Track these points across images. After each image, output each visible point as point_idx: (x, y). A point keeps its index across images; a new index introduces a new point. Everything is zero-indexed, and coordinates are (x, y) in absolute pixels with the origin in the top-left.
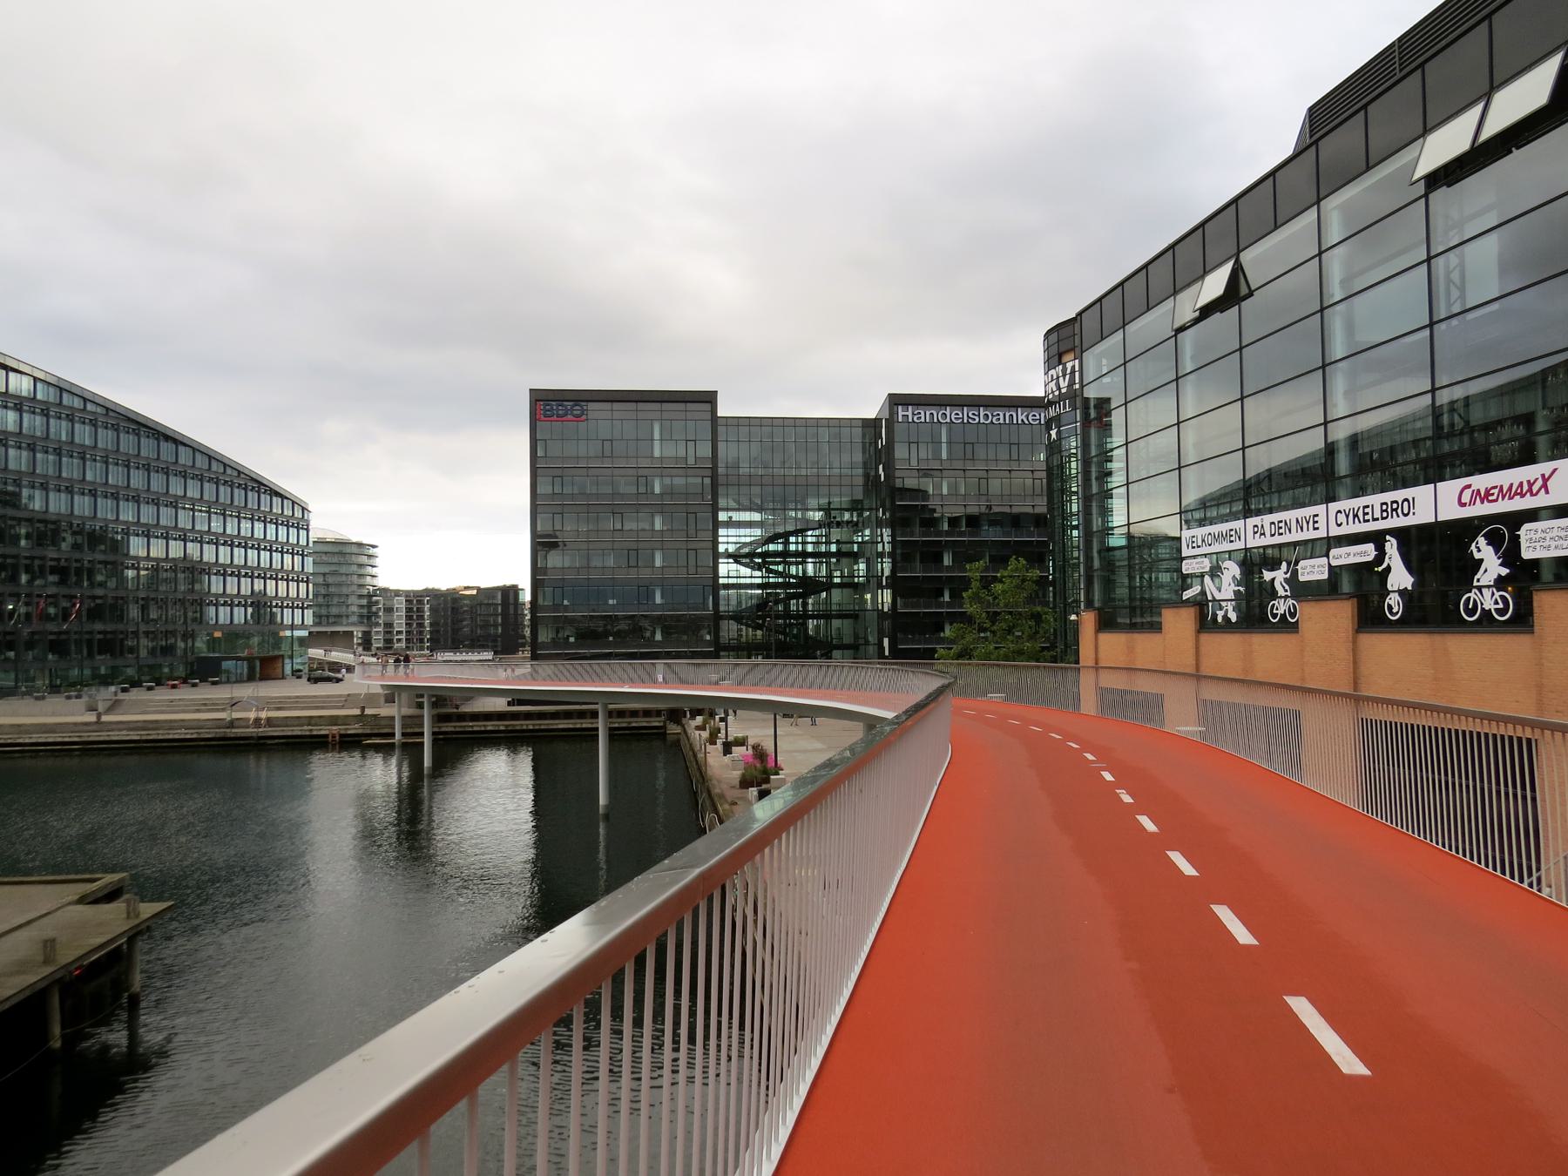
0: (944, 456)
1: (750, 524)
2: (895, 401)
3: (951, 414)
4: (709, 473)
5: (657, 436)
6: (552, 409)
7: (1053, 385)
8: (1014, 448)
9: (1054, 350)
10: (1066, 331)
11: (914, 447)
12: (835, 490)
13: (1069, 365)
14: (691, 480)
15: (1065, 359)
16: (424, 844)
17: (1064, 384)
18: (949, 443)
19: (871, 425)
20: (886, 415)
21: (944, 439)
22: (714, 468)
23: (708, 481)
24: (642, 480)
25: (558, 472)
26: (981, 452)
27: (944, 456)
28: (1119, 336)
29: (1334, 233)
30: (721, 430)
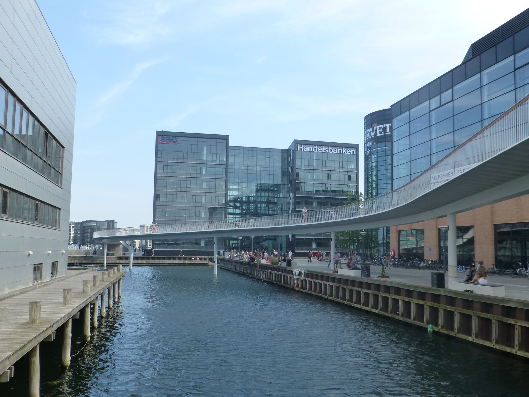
0: (315, 164)
2: (297, 142)
3: (318, 149)
4: (225, 167)
5: (205, 151)
6: (163, 138)
7: (368, 135)
8: (341, 163)
9: (370, 122)
10: (160, 181)
11: (303, 160)
12: (267, 176)
13: (375, 128)
14: (217, 169)
15: (373, 126)
16: (121, 310)
17: (373, 134)
18: (317, 159)
21: (315, 158)
23: (224, 170)
24: (199, 168)
25: (166, 164)
26: (328, 164)
27: (315, 164)
28: (408, 113)
29: (485, 82)
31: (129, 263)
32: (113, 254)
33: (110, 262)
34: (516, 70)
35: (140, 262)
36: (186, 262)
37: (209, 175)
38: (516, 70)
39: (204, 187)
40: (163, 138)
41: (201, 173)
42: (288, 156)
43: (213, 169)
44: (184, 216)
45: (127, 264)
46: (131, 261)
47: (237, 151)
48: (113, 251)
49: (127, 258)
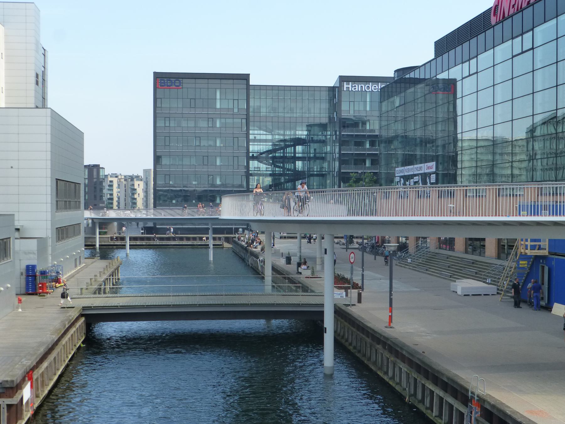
0: (368, 109)
1: (266, 141)
2: (343, 79)
6: (164, 81)
11: (352, 104)
14: (235, 120)
18: (371, 102)
19: (332, 90)
20: (18, 381)
22: (248, 115)
23: (244, 121)
27: (368, 109)
30: (251, 92)
31: (125, 245)
32: (105, 233)
33: (103, 244)
34: (513, 57)
35: (138, 243)
36: (195, 243)
37: (224, 129)
38: (513, 57)
39: (218, 144)
40: (164, 81)
41: (214, 126)
42: (333, 93)
43: (229, 121)
44: (194, 183)
45: (123, 247)
46: (128, 243)
47: (263, 92)
48: (105, 228)
49: (123, 239)
